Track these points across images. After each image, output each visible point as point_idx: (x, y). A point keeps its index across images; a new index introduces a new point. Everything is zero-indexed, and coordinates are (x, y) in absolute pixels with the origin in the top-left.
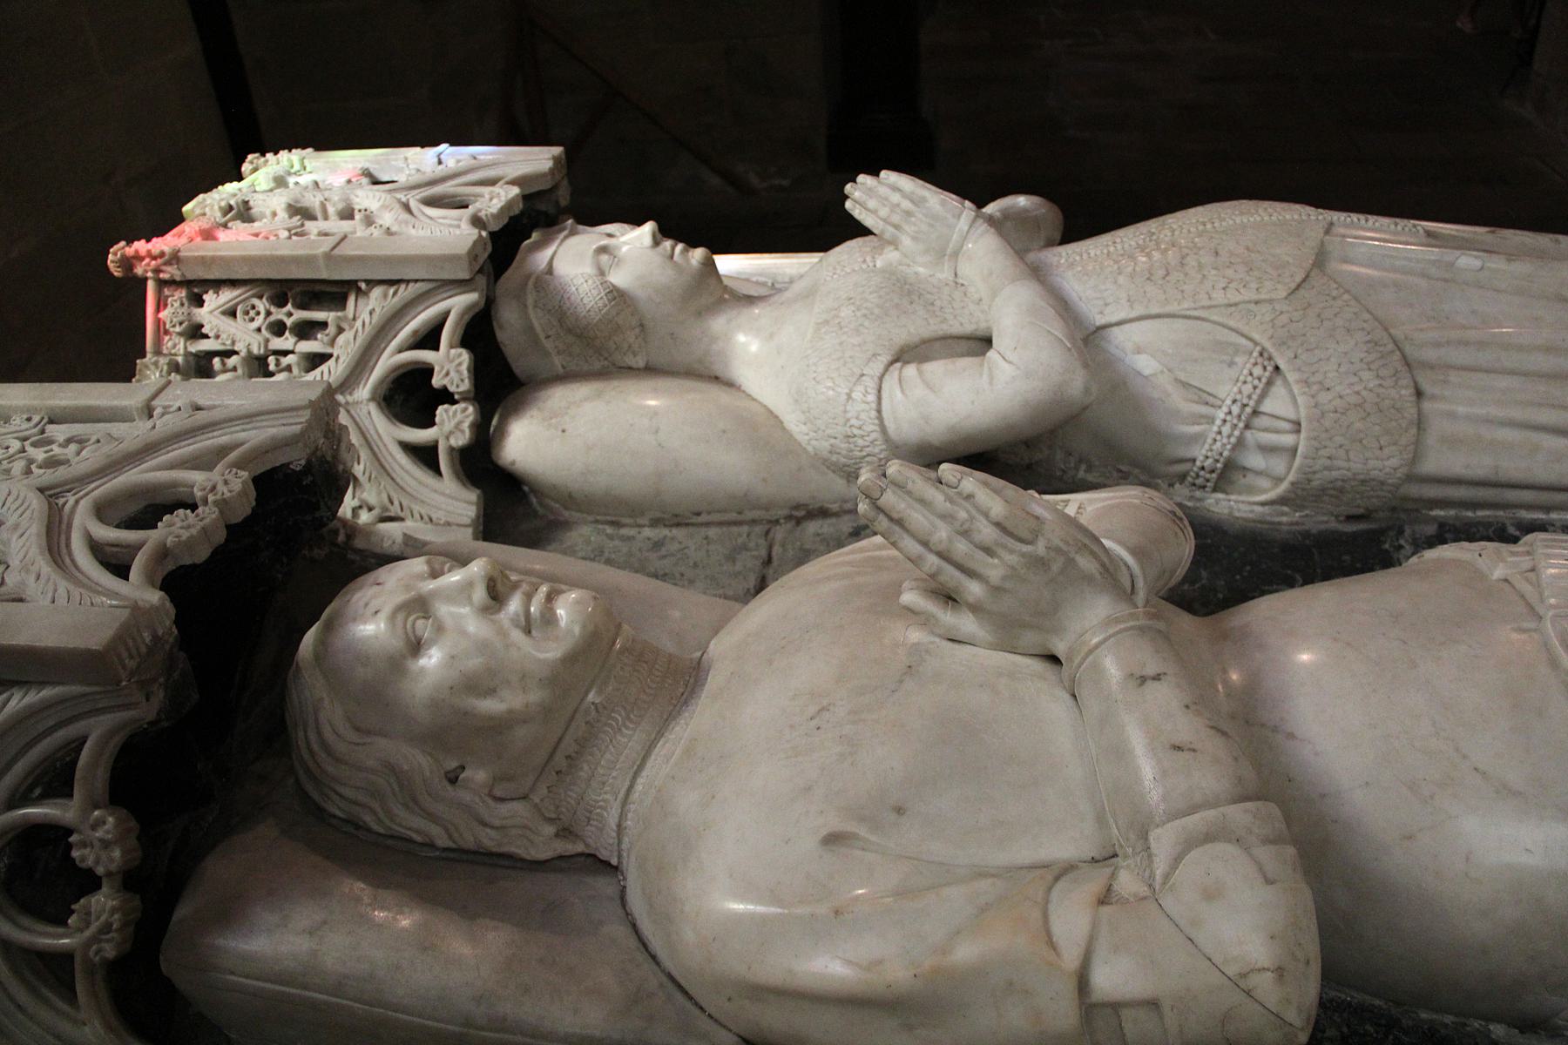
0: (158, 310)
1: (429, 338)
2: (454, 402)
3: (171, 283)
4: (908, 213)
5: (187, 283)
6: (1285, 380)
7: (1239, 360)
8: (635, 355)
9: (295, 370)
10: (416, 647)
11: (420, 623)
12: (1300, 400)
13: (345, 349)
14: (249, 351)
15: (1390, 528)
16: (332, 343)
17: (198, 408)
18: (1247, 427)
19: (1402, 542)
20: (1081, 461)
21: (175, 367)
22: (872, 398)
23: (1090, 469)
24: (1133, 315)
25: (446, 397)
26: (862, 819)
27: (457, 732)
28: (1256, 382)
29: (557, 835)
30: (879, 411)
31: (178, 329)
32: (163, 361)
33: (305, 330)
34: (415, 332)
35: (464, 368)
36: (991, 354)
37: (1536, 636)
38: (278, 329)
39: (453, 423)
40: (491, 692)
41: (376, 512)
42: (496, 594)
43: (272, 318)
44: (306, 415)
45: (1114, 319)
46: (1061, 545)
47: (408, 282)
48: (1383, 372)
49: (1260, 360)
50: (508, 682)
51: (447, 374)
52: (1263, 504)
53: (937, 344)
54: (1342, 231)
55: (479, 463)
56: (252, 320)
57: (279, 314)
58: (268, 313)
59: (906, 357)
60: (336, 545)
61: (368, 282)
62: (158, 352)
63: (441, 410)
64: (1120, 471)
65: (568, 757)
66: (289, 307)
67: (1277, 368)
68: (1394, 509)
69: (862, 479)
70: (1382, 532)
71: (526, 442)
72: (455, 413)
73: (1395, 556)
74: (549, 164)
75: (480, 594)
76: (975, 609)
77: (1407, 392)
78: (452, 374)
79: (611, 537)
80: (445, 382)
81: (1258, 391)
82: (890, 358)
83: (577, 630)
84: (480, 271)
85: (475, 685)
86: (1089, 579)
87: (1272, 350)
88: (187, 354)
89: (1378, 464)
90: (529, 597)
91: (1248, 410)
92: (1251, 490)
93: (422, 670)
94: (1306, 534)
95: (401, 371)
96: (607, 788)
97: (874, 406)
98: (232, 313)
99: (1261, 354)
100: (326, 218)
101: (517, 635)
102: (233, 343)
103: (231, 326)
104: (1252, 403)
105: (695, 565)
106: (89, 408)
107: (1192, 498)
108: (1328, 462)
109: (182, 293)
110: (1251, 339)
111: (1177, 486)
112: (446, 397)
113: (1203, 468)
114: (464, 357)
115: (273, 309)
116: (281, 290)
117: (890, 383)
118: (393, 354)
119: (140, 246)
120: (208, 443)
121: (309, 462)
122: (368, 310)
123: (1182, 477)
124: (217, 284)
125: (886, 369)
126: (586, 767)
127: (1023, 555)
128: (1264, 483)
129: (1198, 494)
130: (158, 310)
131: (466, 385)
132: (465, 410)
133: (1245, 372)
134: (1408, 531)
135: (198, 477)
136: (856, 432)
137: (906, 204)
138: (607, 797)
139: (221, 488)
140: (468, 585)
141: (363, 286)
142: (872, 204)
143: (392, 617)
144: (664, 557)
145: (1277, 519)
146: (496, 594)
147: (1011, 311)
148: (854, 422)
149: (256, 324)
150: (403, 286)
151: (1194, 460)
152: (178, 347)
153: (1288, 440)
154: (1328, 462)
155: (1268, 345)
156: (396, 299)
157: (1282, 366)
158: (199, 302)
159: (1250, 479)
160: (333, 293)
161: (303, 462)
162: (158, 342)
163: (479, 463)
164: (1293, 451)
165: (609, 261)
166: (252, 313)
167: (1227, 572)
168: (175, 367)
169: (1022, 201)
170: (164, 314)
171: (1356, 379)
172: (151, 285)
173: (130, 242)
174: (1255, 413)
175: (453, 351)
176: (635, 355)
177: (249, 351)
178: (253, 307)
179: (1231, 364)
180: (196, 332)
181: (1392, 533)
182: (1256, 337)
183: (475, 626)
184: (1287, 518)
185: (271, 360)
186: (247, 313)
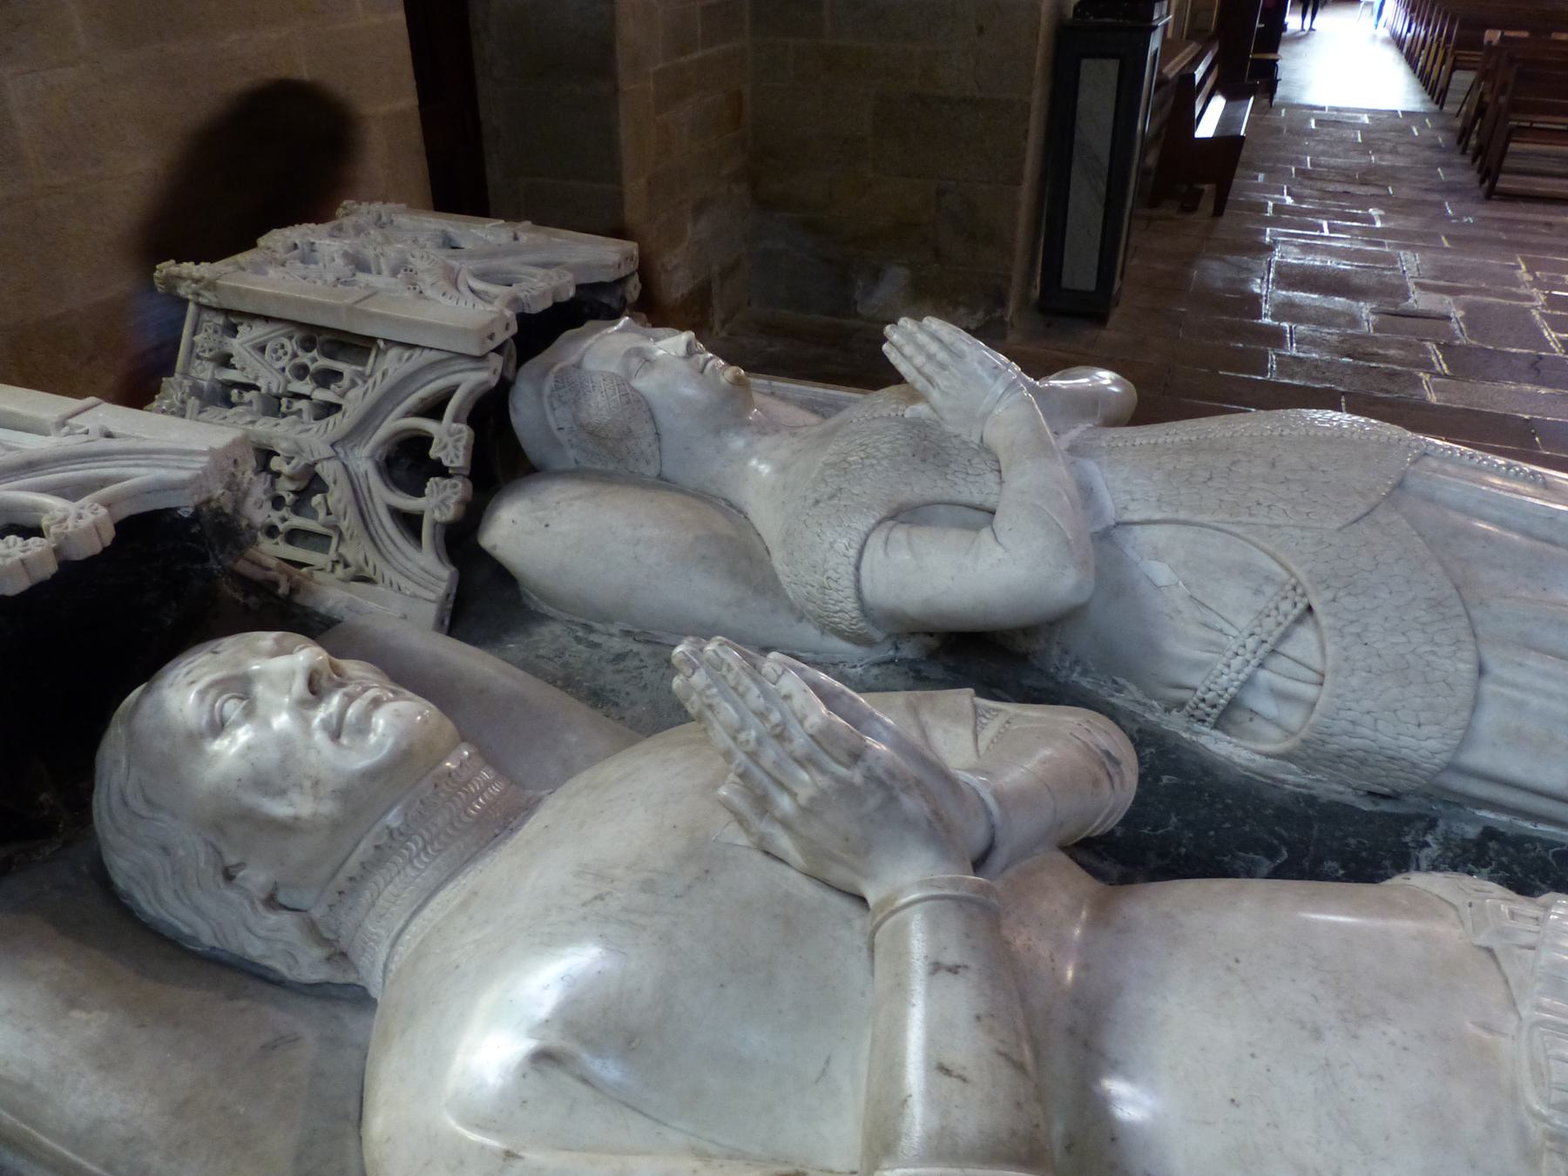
0: (194, 333)
1: (434, 409)
2: (449, 476)
3: (209, 308)
4: (943, 367)
5: (227, 312)
6: (1317, 624)
7: (1270, 590)
8: (648, 462)
9: (305, 416)
10: (219, 727)
12: (1330, 649)
13: (355, 402)
14: (269, 389)
15: (1420, 817)
16: (343, 395)
17: (109, 435)
18: (1261, 666)
19: (1429, 838)
20: (1077, 662)
21: (196, 391)
22: (853, 552)
23: (1085, 673)
24: (1158, 516)
25: (441, 471)
26: (587, 1043)
27: (237, 824)
28: (1281, 618)
29: (328, 959)
30: (858, 568)
31: (207, 355)
32: (186, 383)
33: (327, 378)
34: (423, 400)
35: (461, 445)
36: (985, 534)
38: (301, 372)
40: (281, 793)
41: (352, 570)
42: (316, 689)
43: (297, 361)
44: (205, 460)
45: (1136, 517)
46: (884, 777)
47: (424, 348)
48: (1441, 638)
49: (1291, 594)
50: (301, 787)
51: (445, 447)
52: (1268, 755)
53: (941, 509)
54: (1434, 464)
55: (461, 541)
56: (279, 359)
57: (304, 358)
58: (295, 355)
59: (901, 518)
61: (386, 341)
62: (185, 374)
64: (1115, 682)
65: (351, 879)
66: (315, 353)
67: (1309, 609)
68: (1427, 796)
69: (192, 696)
70: (1408, 820)
71: (518, 530)
73: (1414, 853)
74: (616, 258)
75: (299, 686)
76: (786, 824)
77: (1466, 668)
78: (450, 446)
79: (578, 640)
80: (441, 455)
81: (1282, 628)
82: (884, 514)
83: (389, 742)
84: (498, 350)
85: (264, 781)
86: (909, 824)
87: (1307, 585)
88: (213, 379)
89: (1413, 742)
90: (350, 698)
91: (1267, 647)
92: (1255, 736)
93: (217, 755)
94: (1311, 800)
95: (405, 435)
96: (383, 923)
97: (853, 560)
98: (262, 349)
99: (1294, 589)
100: (379, 273)
101: (320, 738)
102: (256, 378)
103: (261, 360)
104: (1271, 640)
105: (645, 687)
106: (12, 414)
107: (1188, 729)
108: (1350, 727)
109: (220, 320)
110: (1288, 570)
111: (1174, 712)
112: (441, 471)
113: (1203, 700)
114: (466, 432)
115: (300, 352)
116: (311, 335)
117: (876, 541)
118: (408, 414)
119: (188, 268)
120: (91, 472)
121: (197, 509)
122: (392, 365)
123: (1181, 705)
124: (253, 317)
125: (873, 529)
126: (368, 894)
127: (838, 779)
128: (1272, 732)
129: (1197, 726)
130: (194, 333)
132: (455, 486)
133: (1272, 605)
134: (1442, 824)
135: (55, 503)
136: (833, 585)
137: (942, 356)
138: (383, 932)
139: (70, 523)
140: (291, 675)
141: (382, 344)
142: (908, 350)
143: (202, 694)
144: (619, 672)
145: (1282, 776)
146: (316, 689)
147: (1029, 485)
148: (831, 573)
149: (279, 364)
150: (418, 352)
151: (1195, 690)
152: (206, 374)
153: (1310, 691)
154: (1350, 727)
155: (1303, 578)
156: (410, 363)
157: (1315, 606)
158: (233, 330)
159: (1258, 725)
160: (355, 346)
161: (191, 510)
162: (188, 363)
163: (461, 541)
164: (1312, 705)
165: (663, 364)
166: (281, 352)
167: (1187, 825)
168: (196, 391)
169: (1106, 377)
170: (199, 337)
171: (1404, 639)
172: (191, 307)
173: (179, 261)
174: (1273, 651)
176: (648, 462)
177: (269, 389)
178: (283, 346)
179: (1258, 592)
180: (225, 361)
181: (1420, 825)
182: (1294, 568)
183: (282, 721)
184: (1292, 777)
185: (284, 401)
186: (275, 351)
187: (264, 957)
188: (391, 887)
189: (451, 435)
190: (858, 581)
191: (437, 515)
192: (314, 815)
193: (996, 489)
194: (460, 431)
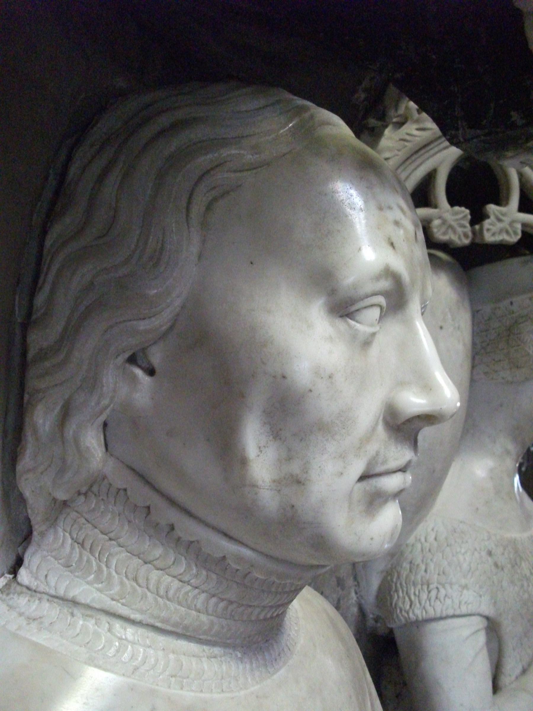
2: (473, 223)
11: (375, 313)
22: (464, 610)
30: (454, 616)
37: (121, 491)
39: (454, 224)
50: (289, 459)
51: (499, 220)
60: (365, 117)
63: (464, 212)
65: (172, 528)
72: (464, 227)
78: (499, 225)
97: (458, 612)
112: (478, 217)
126: (158, 552)
131: (489, 238)
132: (466, 235)
136: (433, 594)
148: (443, 592)
175: (519, 227)
187: (35, 431)
188: (176, 584)
189: (511, 224)
190: (441, 618)
191: (436, 222)
192: (254, 486)
193: (513, 677)
194: (515, 233)
